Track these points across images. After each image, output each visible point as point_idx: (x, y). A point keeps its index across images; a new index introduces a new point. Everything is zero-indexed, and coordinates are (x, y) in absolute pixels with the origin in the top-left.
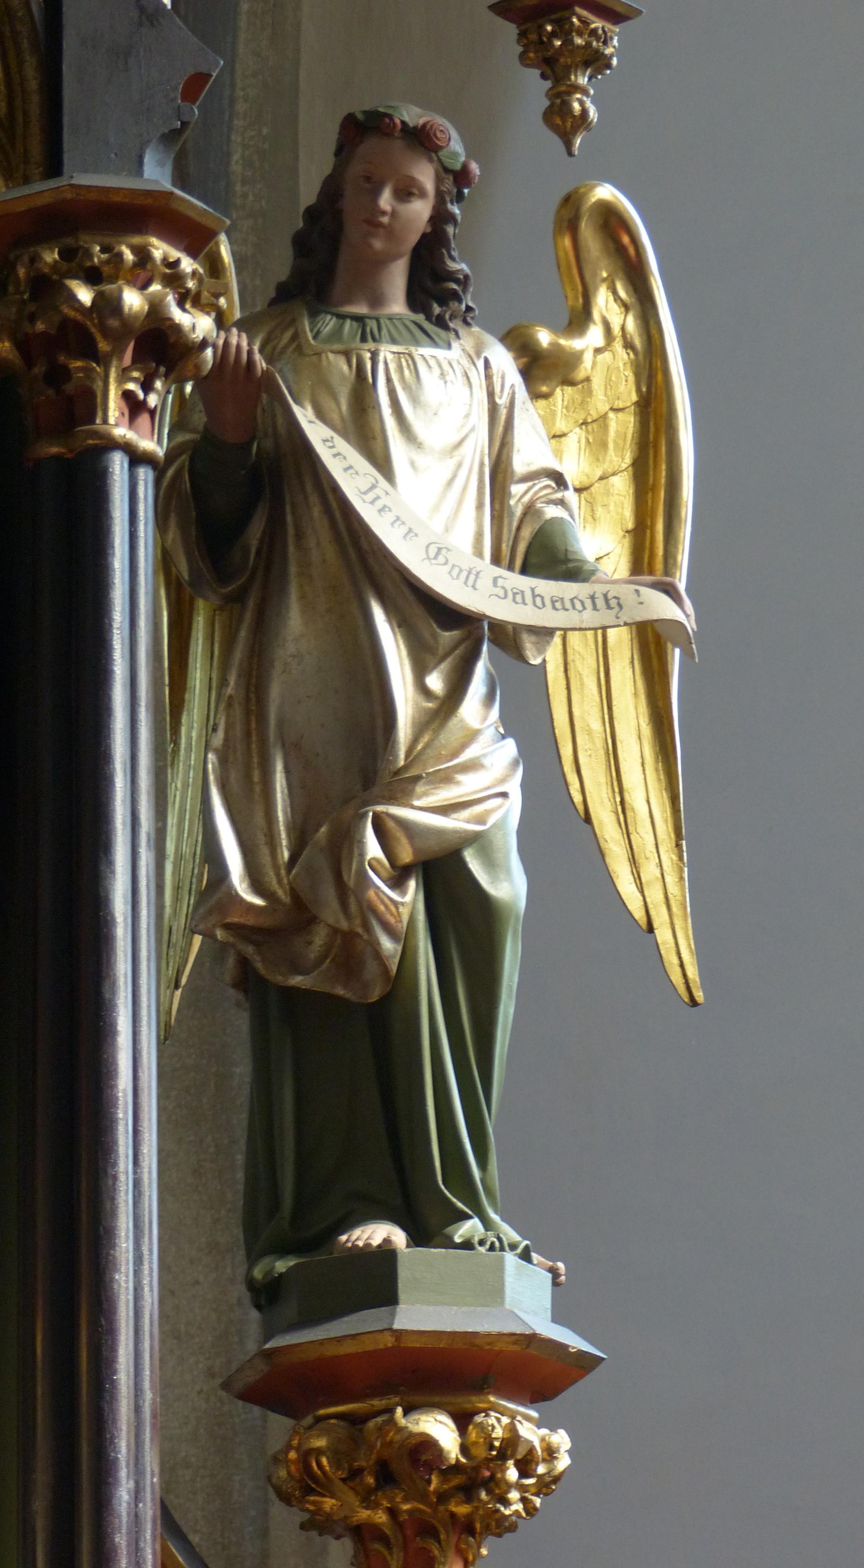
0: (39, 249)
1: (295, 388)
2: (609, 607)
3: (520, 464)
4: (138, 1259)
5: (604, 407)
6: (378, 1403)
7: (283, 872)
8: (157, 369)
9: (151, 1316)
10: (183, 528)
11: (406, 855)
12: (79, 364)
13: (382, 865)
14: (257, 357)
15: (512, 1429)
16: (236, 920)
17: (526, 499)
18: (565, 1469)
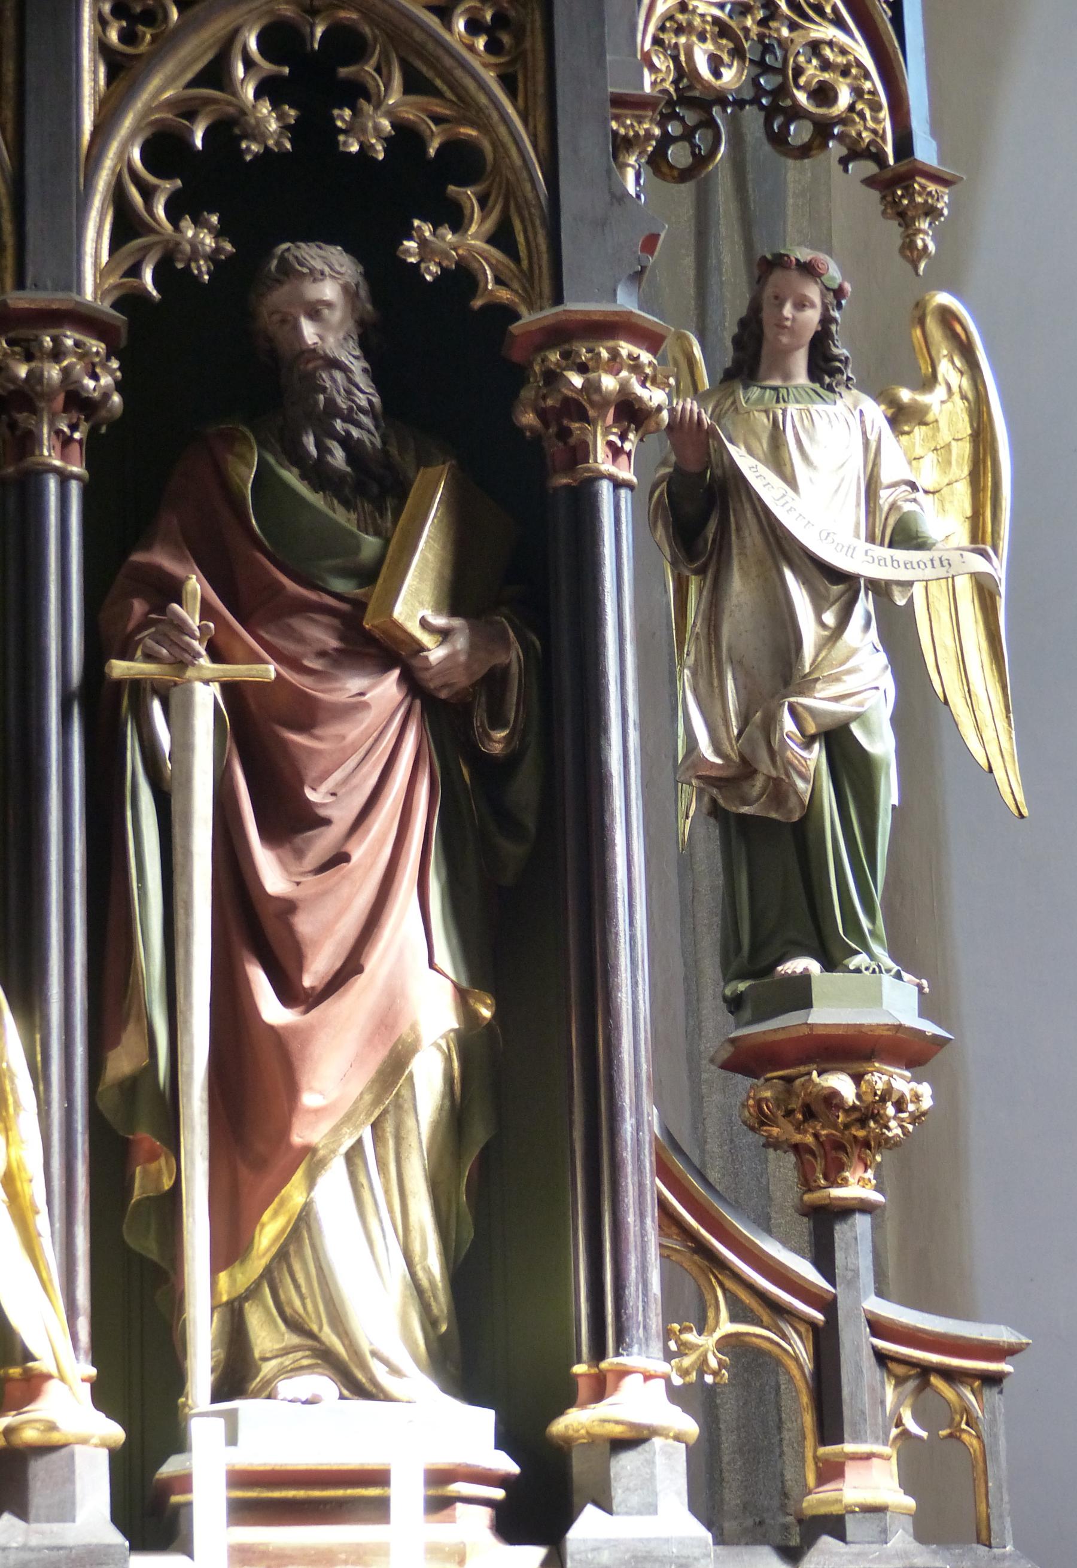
0: (547, 353)
1: (733, 435)
2: (942, 566)
3: (886, 476)
4: (635, 984)
5: (948, 438)
6: (803, 1069)
7: (734, 742)
8: (629, 426)
9: (645, 1018)
10: (666, 527)
11: (812, 729)
12: (577, 425)
13: (796, 735)
14: (704, 416)
15: (889, 1083)
16: (704, 773)
17: (891, 500)
18: (929, 1108)
